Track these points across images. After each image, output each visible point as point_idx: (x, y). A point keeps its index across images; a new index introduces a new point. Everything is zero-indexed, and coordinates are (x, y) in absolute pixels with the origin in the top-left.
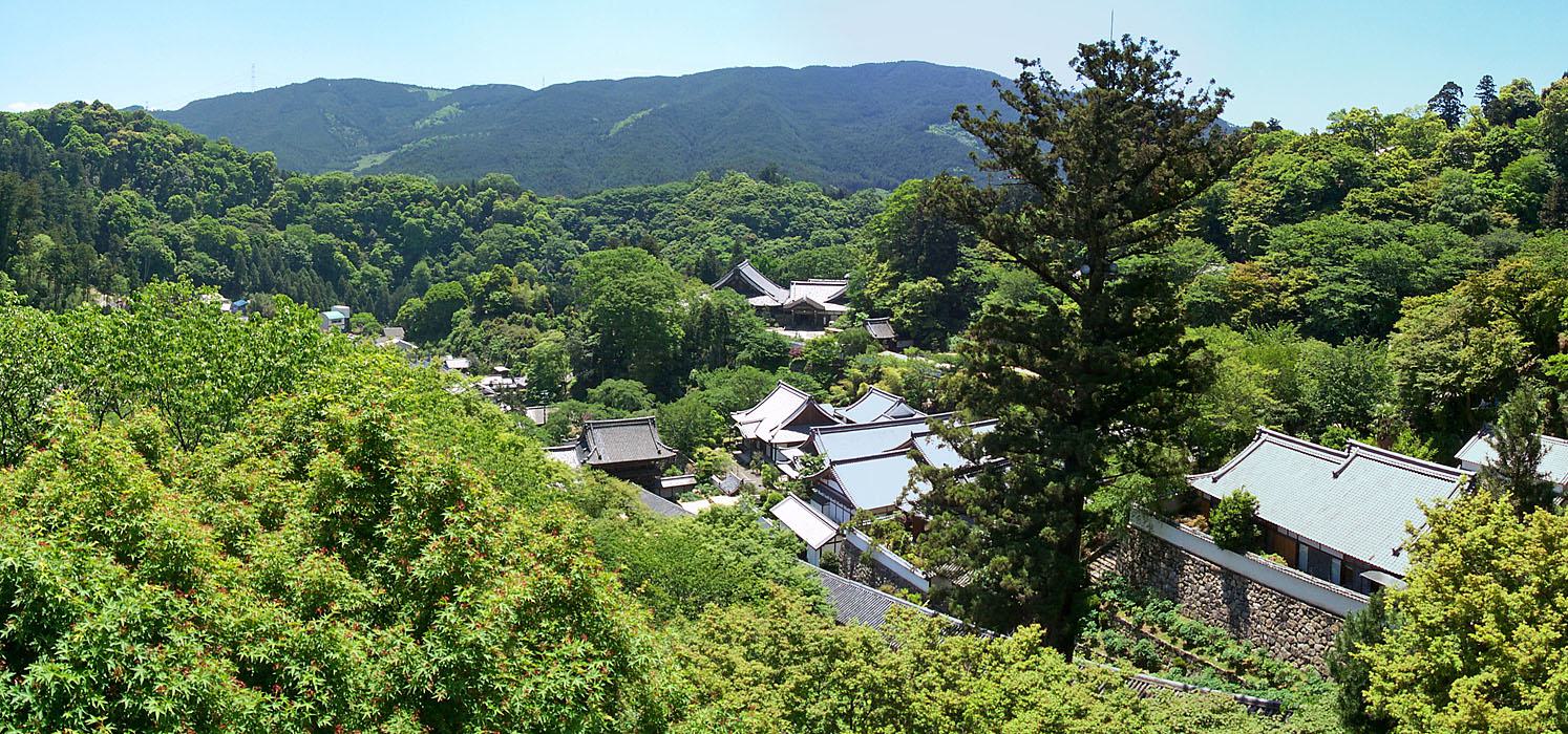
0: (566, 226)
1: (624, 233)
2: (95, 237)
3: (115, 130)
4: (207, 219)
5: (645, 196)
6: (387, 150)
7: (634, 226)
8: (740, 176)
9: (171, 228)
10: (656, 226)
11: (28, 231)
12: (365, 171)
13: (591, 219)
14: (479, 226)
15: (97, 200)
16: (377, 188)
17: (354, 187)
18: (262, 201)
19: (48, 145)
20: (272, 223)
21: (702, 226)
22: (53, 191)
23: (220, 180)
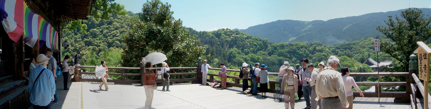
0: (333, 52)
1: (346, 53)
2: (228, 59)
3: (232, 35)
4: (253, 54)
5: (350, 44)
6: (296, 36)
7: (348, 51)
8: (371, 38)
9: (245, 56)
10: (353, 51)
11: (213, 58)
12: (291, 41)
13: (338, 50)
14: (313, 53)
15: (228, 51)
16: (292, 45)
17: (287, 46)
18: (265, 50)
19: (217, 39)
20: (268, 55)
21: (363, 50)
22: (218, 49)
23: (256, 45)
